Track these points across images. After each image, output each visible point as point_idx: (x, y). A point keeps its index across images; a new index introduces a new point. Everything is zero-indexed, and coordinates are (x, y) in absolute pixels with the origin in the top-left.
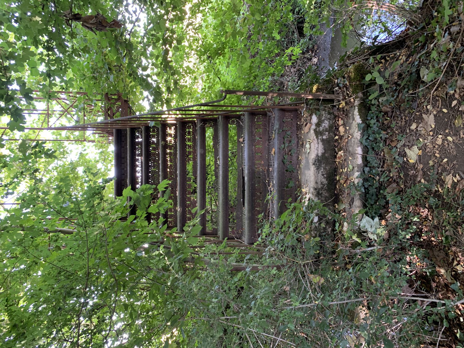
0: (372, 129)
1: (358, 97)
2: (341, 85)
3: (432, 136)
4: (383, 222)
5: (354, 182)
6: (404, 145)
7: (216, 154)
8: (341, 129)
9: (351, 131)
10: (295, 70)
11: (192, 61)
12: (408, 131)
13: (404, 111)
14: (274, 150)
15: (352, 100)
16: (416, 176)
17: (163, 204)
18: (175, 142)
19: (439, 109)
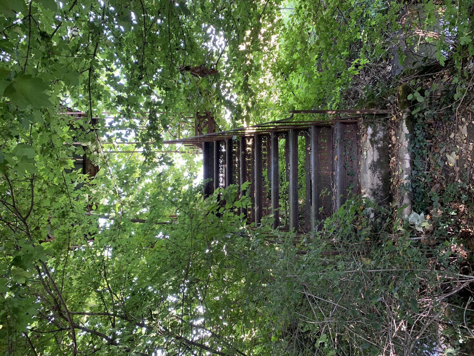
0: (418, 138)
1: (405, 112)
2: (392, 102)
3: (466, 143)
4: (428, 217)
5: (403, 183)
6: (445, 152)
7: (287, 161)
8: (393, 138)
9: (401, 141)
10: (370, 78)
11: (267, 78)
12: (448, 140)
13: (445, 122)
14: (336, 157)
15: (401, 114)
16: (455, 177)
17: (244, 202)
18: (253, 151)
19: (470, 122)
